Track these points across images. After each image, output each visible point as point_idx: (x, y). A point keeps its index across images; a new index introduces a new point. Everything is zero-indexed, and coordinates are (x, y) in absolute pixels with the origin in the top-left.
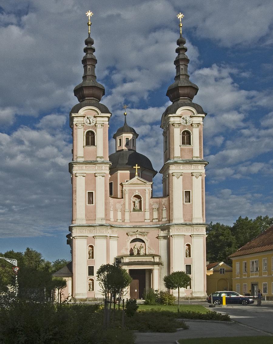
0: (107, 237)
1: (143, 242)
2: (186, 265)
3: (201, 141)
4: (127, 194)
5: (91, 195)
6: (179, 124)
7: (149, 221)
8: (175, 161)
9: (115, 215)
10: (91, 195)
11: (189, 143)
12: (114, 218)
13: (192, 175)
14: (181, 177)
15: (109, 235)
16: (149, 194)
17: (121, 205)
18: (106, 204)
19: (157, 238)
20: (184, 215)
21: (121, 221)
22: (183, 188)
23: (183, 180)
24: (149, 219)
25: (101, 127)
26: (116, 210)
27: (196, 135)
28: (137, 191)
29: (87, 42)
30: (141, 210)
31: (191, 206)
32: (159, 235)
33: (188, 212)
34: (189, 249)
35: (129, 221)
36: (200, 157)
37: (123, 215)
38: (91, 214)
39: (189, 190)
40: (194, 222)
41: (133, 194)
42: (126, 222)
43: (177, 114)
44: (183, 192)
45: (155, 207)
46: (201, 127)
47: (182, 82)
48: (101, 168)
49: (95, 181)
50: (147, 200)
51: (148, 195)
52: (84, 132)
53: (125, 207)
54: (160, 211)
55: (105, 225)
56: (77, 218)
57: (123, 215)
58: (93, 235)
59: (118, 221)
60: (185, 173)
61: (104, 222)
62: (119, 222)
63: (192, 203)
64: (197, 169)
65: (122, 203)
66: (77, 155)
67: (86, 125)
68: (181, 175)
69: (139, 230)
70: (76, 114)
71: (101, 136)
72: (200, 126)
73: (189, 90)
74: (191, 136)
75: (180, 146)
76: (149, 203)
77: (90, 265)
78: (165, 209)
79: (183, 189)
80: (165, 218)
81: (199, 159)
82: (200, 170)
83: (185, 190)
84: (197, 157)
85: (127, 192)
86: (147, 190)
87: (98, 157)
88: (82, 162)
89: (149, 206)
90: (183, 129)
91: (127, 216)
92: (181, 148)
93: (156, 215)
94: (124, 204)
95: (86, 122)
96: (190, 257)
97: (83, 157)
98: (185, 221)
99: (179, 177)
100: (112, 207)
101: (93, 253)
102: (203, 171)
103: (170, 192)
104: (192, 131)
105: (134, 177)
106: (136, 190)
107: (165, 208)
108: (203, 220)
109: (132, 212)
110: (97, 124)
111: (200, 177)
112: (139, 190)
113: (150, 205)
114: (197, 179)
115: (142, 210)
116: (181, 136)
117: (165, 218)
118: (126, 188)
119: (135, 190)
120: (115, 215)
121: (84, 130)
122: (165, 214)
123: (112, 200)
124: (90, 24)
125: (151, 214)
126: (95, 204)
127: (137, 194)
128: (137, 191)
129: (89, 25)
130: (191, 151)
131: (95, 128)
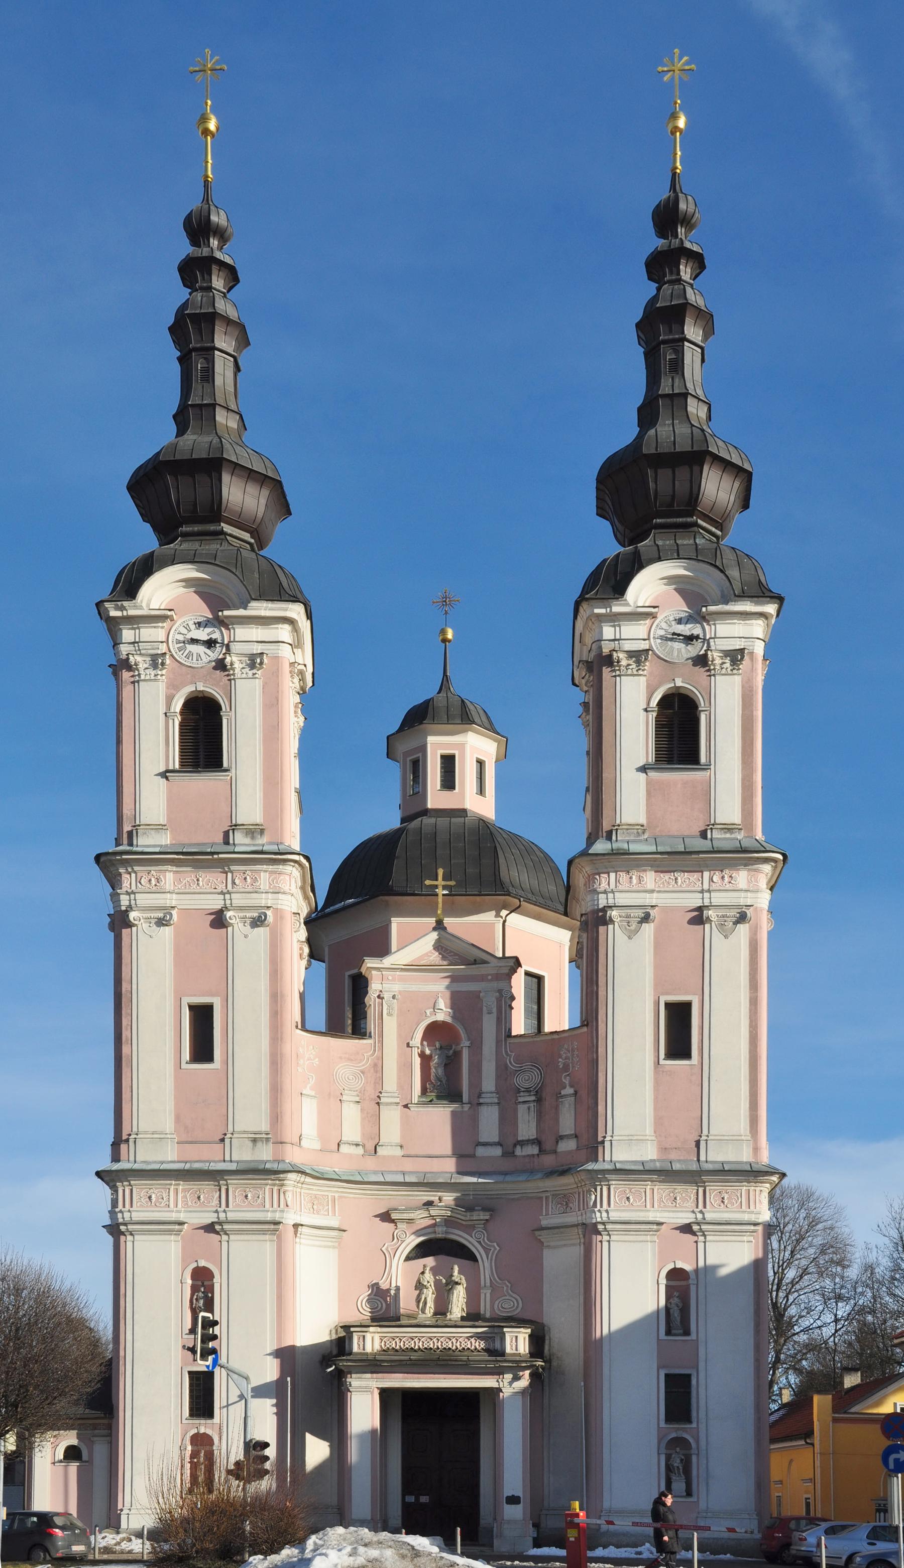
2: (667, 1375)
4: (389, 1014)
5: (202, 1017)
6: (638, 656)
7: (498, 1151)
8: (615, 846)
12: (322, 1136)
17: (363, 1072)
20: (659, 1122)
21: (360, 1151)
22: (659, 985)
24: (496, 1140)
26: (331, 1099)
33: (687, 1112)
35: (398, 1152)
37: (373, 1119)
38: (205, 1115)
39: (686, 993)
40: (716, 1154)
42: (384, 1156)
43: (631, 603)
45: (527, 1085)
47: (668, 433)
52: (169, 700)
55: (268, 1166)
58: (207, 1215)
59: (344, 1149)
62: (351, 1156)
64: (728, 887)
70: (125, 604)
71: (266, 727)
72: (745, 664)
74: (703, 718)
79: (655, 989)
82: (743, 894)
83: (667, 994)
84: (729, 828)
88: (157, 850)
89: (498, 1077)
91: (392, 1123)
93: (527, 1128)
94: (378, 1068)
96: (687, 1332)
98: (663, 1149)
100: (312, 1082)
107: (571, 1086)
108: (756, 1150)
109: (413, 1108)
113: (503, 1072)
114: (726, 937)
115: (465, 1098)
120: (329, 1121)
121: (167, 688)
124: (212, 125)
125: (507, 1120)
129: (206, 132)
130: (706, 796)
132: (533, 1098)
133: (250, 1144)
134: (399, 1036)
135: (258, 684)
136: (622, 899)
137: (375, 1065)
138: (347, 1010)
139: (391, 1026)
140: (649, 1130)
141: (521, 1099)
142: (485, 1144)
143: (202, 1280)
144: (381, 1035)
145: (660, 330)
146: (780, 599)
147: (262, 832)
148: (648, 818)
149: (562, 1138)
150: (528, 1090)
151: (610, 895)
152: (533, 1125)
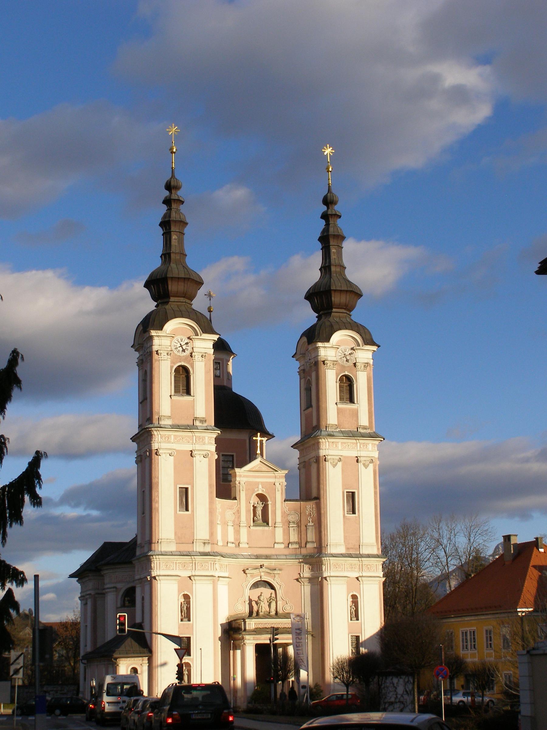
0: (214, 578)
1: (272, 587)
3: (371, 399)
4: (243, 490)
5: (185, 492)
7: (282, 546)
9: (225, 534)
10: (185, 492)
11: (351, 400)
12: (222, 540)
13: (357, 461)
14: (340, 464)
15: (217, 574)
16: (282, 493)
18: (212, 512)
19: (297, 580)
20: (345, 538)
21: (234, 545)
22: (344, 486)
23: (343, 471)
25: (201, 359)
26: (225, 524)
27: (362, 383)
28: (260, 486)
29: (169, 187)
30: (268, 524)
31: (358, 522)
32: (302, 575)
33: (352, 532)
34: (188, 603)
35: (247, 546)
36: (370, 427)
37: (237, 532)
38: (185, 532)
39: (353, 489)
41: (254, 491)
44: (343, 493)
46: (370, 370)
48: (203, 440)
49: (192, 464)
50: (279, 508)
51: (279, 496)
52: (172, 367)
53: (239, 517)
54: (303, 527)
56: (160, 538)
57: (237, 532)
59: (229, 545)
60: (345, 457)
61: (208, 549)
62: (231, 547)
63: (359, 516)
65: (235, 510)
66: (159, 413)
67: (176, 355)
68: (340, 460)
69: (266, 562)
73: (348, 297)
75: (336, 404)
76: (282, 509)
77: (185, 634)
78: (311, 524)
80: (313, 542)
81: (368, 431)
84: (365, 428)
85: (243, 487)
86: (277, 484)
87: (195, 419)
89: (282, 516)
90: (341, 373)
91: (244, 532)
92: (338, 409)
94: (239, 511)
95: (175, 349)
96: (358, 619)
97: (169, 417)
98: (347, 549)
99: (337, 464)
101: (188, 609)
102: (376, 454)
103: (322, 492)
104: (356, 377)
105: (255, 458)
106: (259, 485)
110: (195, 354)
111: (371, 466)
112: (262, 483)
113: (284, 514)
115: (270, 525)
116: (338, 384)
117: (313, 542)
118: (242, 479)
119: (257, 484)
120: (225, 534)
122: (311, 535)
123: (221, 503)
124: (174, 150)
125: (287, 533)
126: (193, 511)
127: (260, 492)
128: (260, 486)
129: (172, 152)
131: (191, 361)
132: (295, 525)
133: (203, 545)
134: (246, 499)
135: (203, 363)
136: (331, 452)
137: (238, 511)
138: (225, 488)
139: (242, 496)
140: (342, 541)
141: (291, 526)
142: (278, 543)
143: (354, 597)
144: (240, 499)
145: (329, 241)
146: (379, 346)
147: (206, 421)
148: (338, 422)
149: (309, 542)
150: (294, 522)
151: (327, 451)
152: (296, 536)
